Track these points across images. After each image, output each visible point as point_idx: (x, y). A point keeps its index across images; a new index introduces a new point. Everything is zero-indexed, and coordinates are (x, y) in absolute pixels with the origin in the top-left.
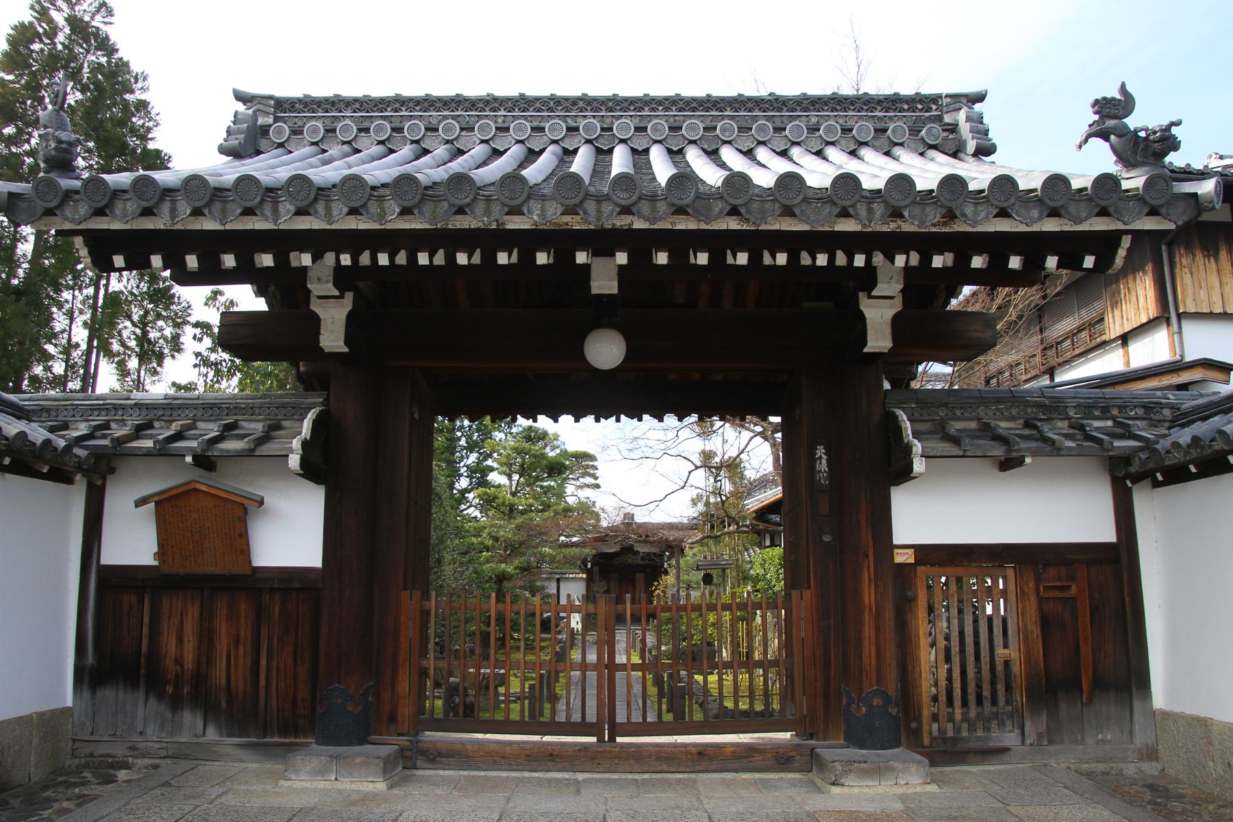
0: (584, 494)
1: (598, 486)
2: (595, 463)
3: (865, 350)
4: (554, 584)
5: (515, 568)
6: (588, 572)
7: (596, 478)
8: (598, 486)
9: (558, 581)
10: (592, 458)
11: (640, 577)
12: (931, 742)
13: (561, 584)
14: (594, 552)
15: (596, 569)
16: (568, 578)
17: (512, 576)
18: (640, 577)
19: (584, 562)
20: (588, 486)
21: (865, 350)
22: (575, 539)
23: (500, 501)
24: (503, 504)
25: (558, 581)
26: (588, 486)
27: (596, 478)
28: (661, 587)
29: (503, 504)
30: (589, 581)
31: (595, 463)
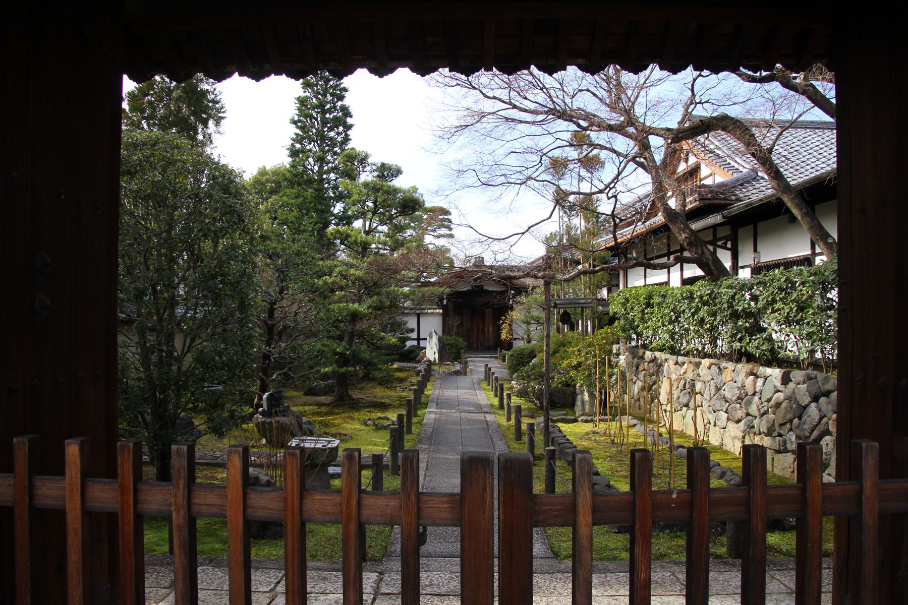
0: (441, 242)
1: (452, 236)
2: (450, 217)
3: (125, 77)
4: (415, 319)
5: (368, 308)
6: (444, 308)
7: (450, 229)
8: (452, 236)
9: (418, 316)
10: (446, 212)
11: (489, 312)
12: (212, 187)
13: (422, 319)
14: (448, 290)
15: (451, 305)
16: (427, 313)
17: (365, 315)
18: (489, 312)
19: (441, 300)
20: (443, 236)
21: (125, 77)
22: (432, 280)
23: (352, 239)
24: (356, 241)
25: (418, 316)
26: (443, 236)
27: (450, 229)
28: (508, 321)
29: (356, 241)
30: (445, 316)
31: (450, 217)
